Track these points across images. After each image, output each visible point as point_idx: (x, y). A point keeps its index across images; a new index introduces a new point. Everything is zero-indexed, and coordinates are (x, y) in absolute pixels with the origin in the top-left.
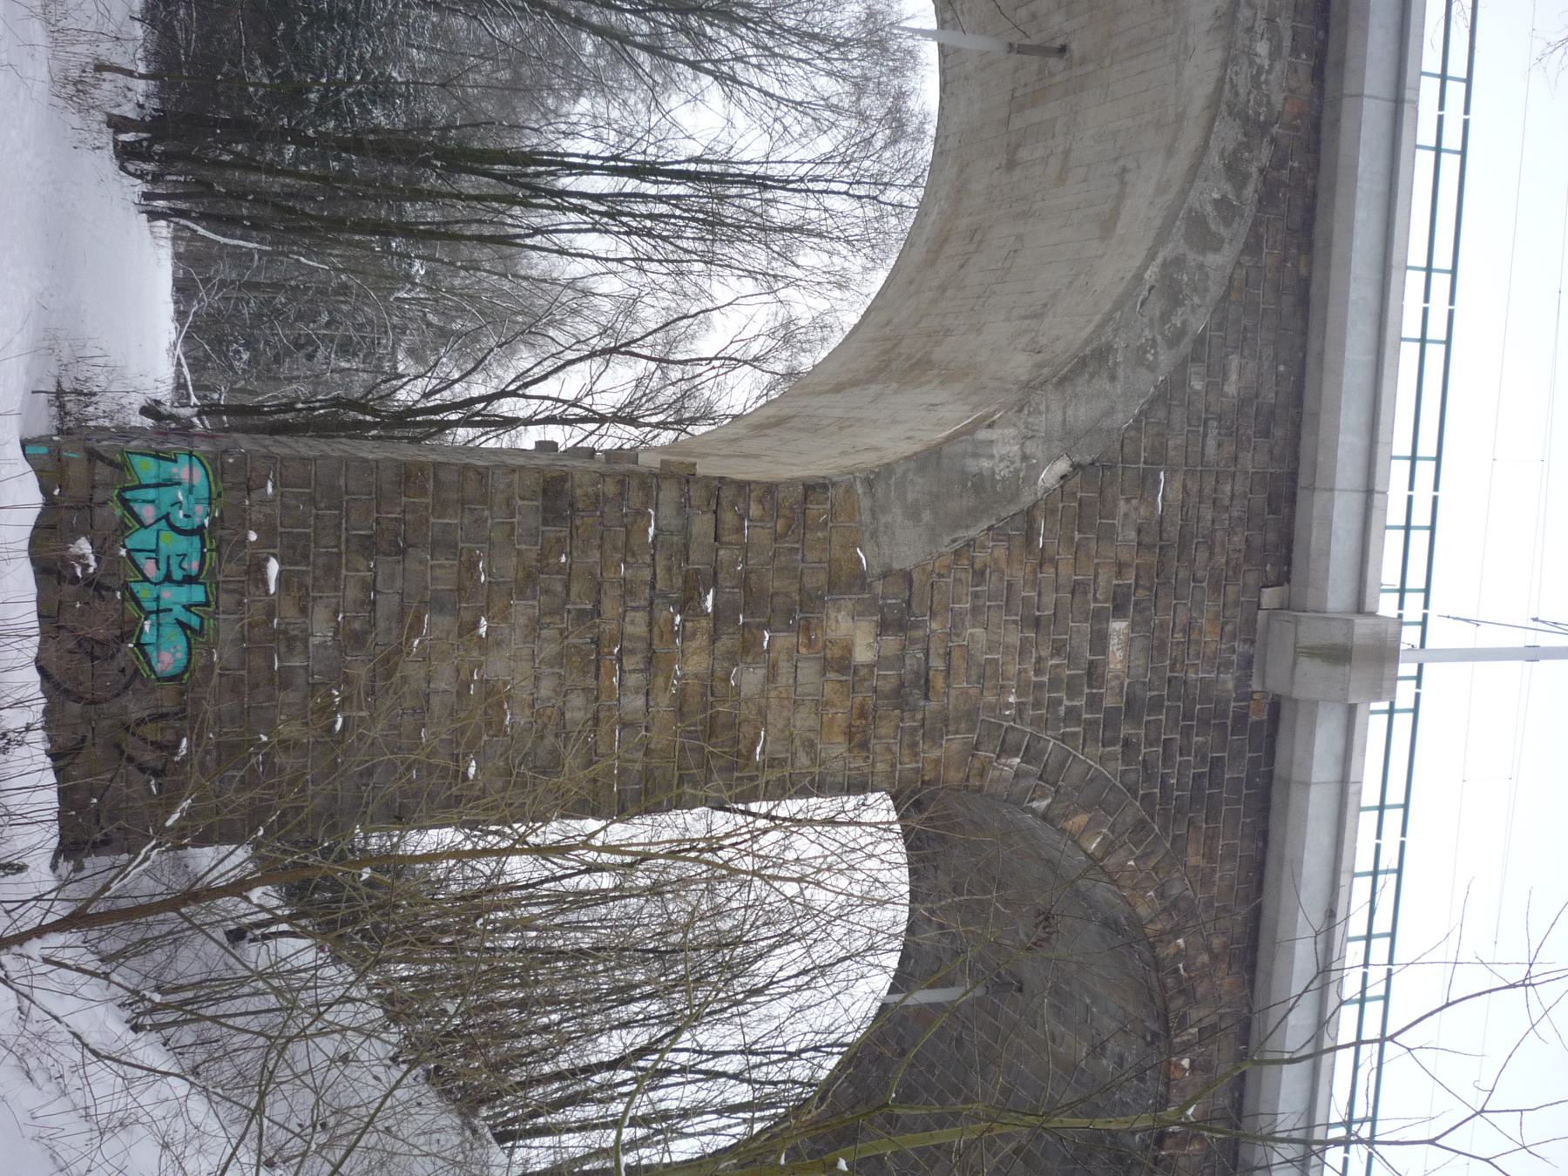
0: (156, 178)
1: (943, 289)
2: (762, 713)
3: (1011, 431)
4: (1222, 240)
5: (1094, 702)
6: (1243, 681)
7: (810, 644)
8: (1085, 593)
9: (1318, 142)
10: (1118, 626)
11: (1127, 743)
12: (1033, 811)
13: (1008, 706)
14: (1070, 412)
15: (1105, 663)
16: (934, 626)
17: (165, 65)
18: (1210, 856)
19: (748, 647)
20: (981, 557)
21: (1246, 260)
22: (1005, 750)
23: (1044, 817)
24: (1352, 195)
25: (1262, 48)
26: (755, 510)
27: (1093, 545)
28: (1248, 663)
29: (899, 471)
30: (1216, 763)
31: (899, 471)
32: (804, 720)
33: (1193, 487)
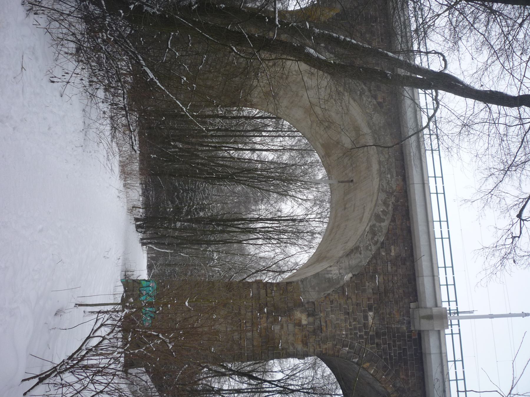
0: (145, 233)
1: (331, 240)
2: (280, 336)
3: (336, 268)
4: (385, 220)
5: (366, 333)
6: (409, 327)
7: (291, 320)
8: (360, 306)
9: (407, 195)
10: (371, 314)
11: (377, 344)
12: (354, 362)
13: (343, 334)
14: (350, 262)
15: (368, 323)
16: (322, 315)
17: (146, 205)
18: (407, 375)
19: (276, 321)
20: (332, 298)
21: (392, 223)
22: (344, 346)
23: (357, 363)
24: (416, 206)
25: (389, 176)
26: (275, 289)
27: (361, 294)
28: (409, 323)
29: (309, 278)
30: (405, 350)
31: (309, 278)
32: (291, 338)
33: (386, 278)
